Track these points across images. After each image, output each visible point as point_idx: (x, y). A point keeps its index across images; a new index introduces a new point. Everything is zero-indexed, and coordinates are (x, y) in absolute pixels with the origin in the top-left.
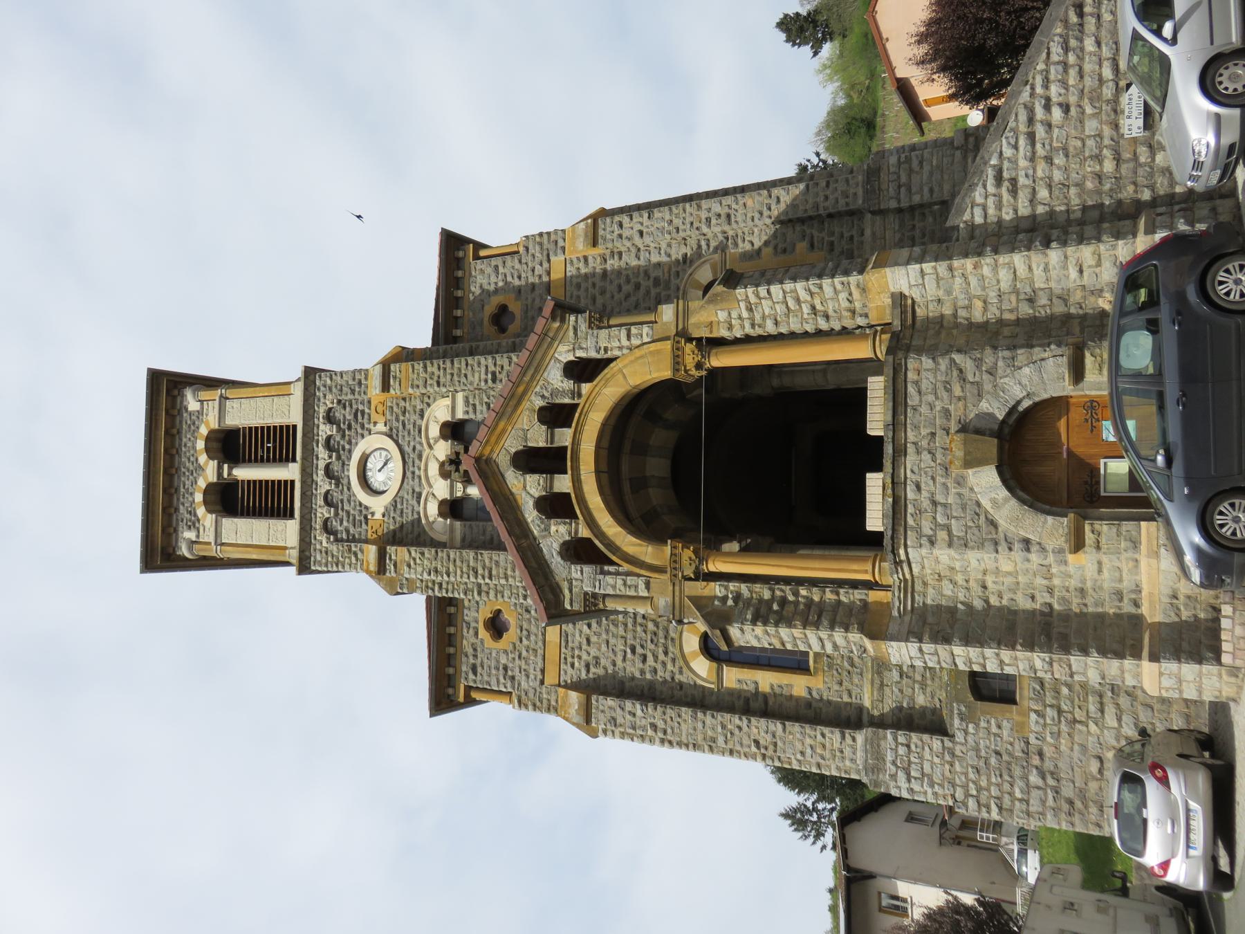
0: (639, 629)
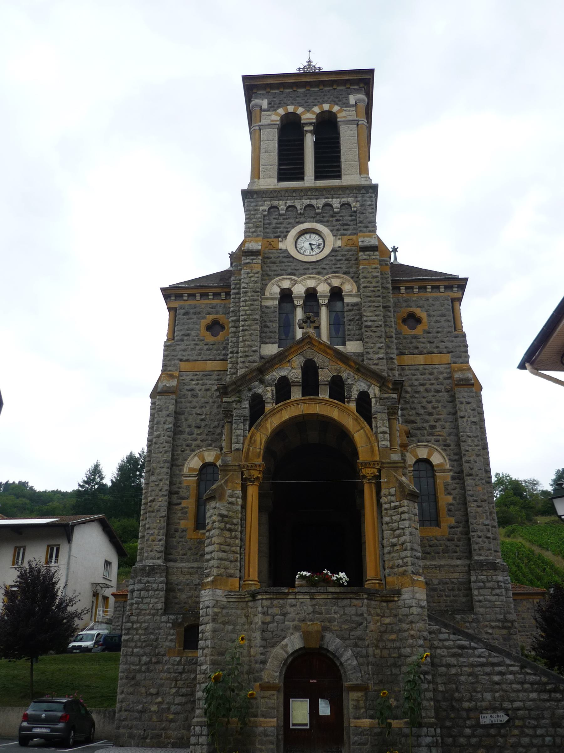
0: (216, 423)
